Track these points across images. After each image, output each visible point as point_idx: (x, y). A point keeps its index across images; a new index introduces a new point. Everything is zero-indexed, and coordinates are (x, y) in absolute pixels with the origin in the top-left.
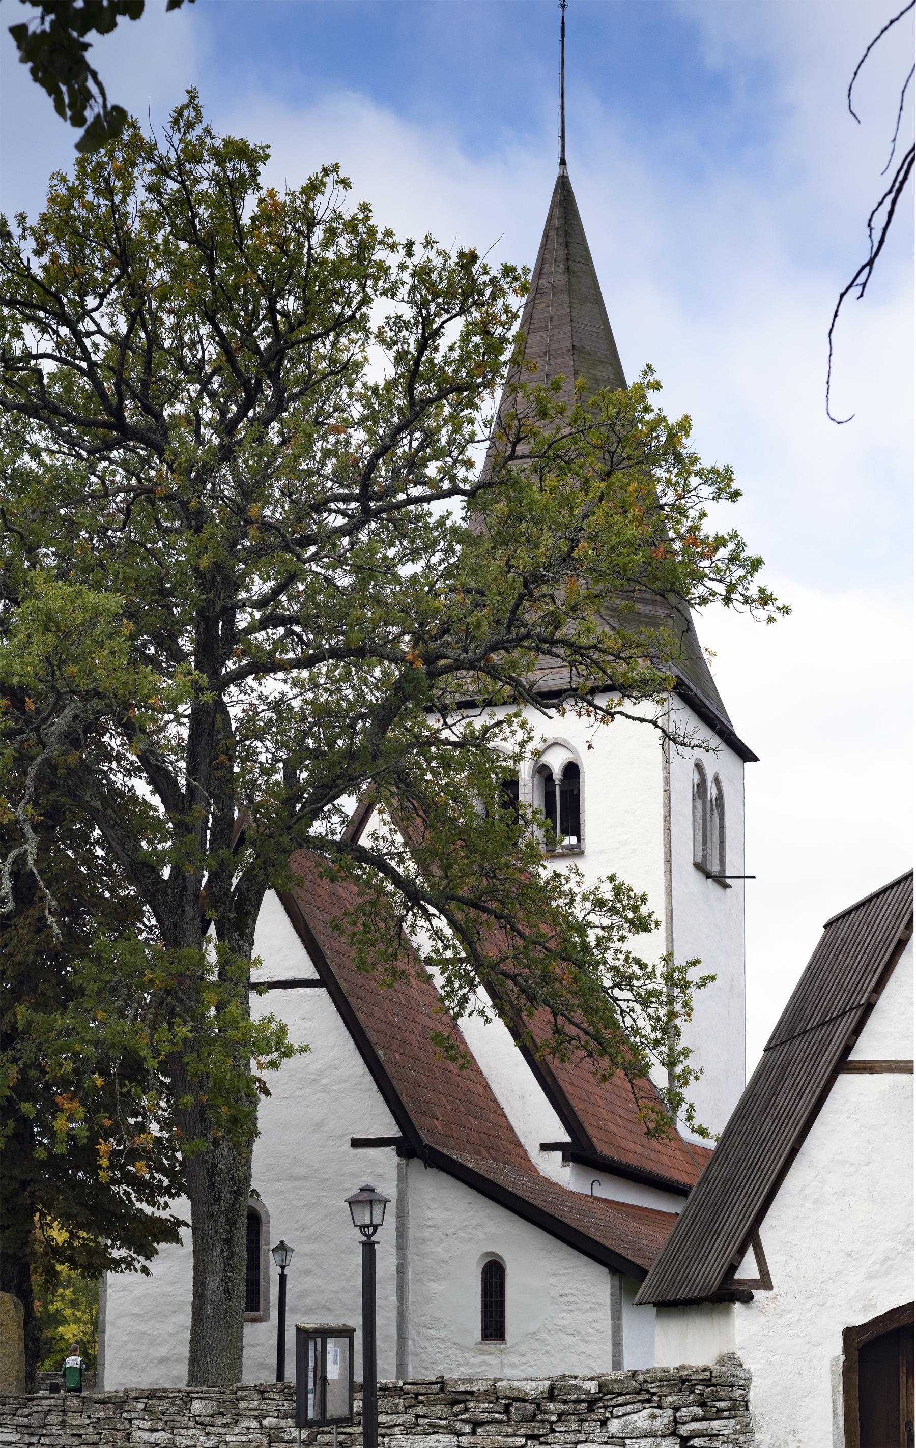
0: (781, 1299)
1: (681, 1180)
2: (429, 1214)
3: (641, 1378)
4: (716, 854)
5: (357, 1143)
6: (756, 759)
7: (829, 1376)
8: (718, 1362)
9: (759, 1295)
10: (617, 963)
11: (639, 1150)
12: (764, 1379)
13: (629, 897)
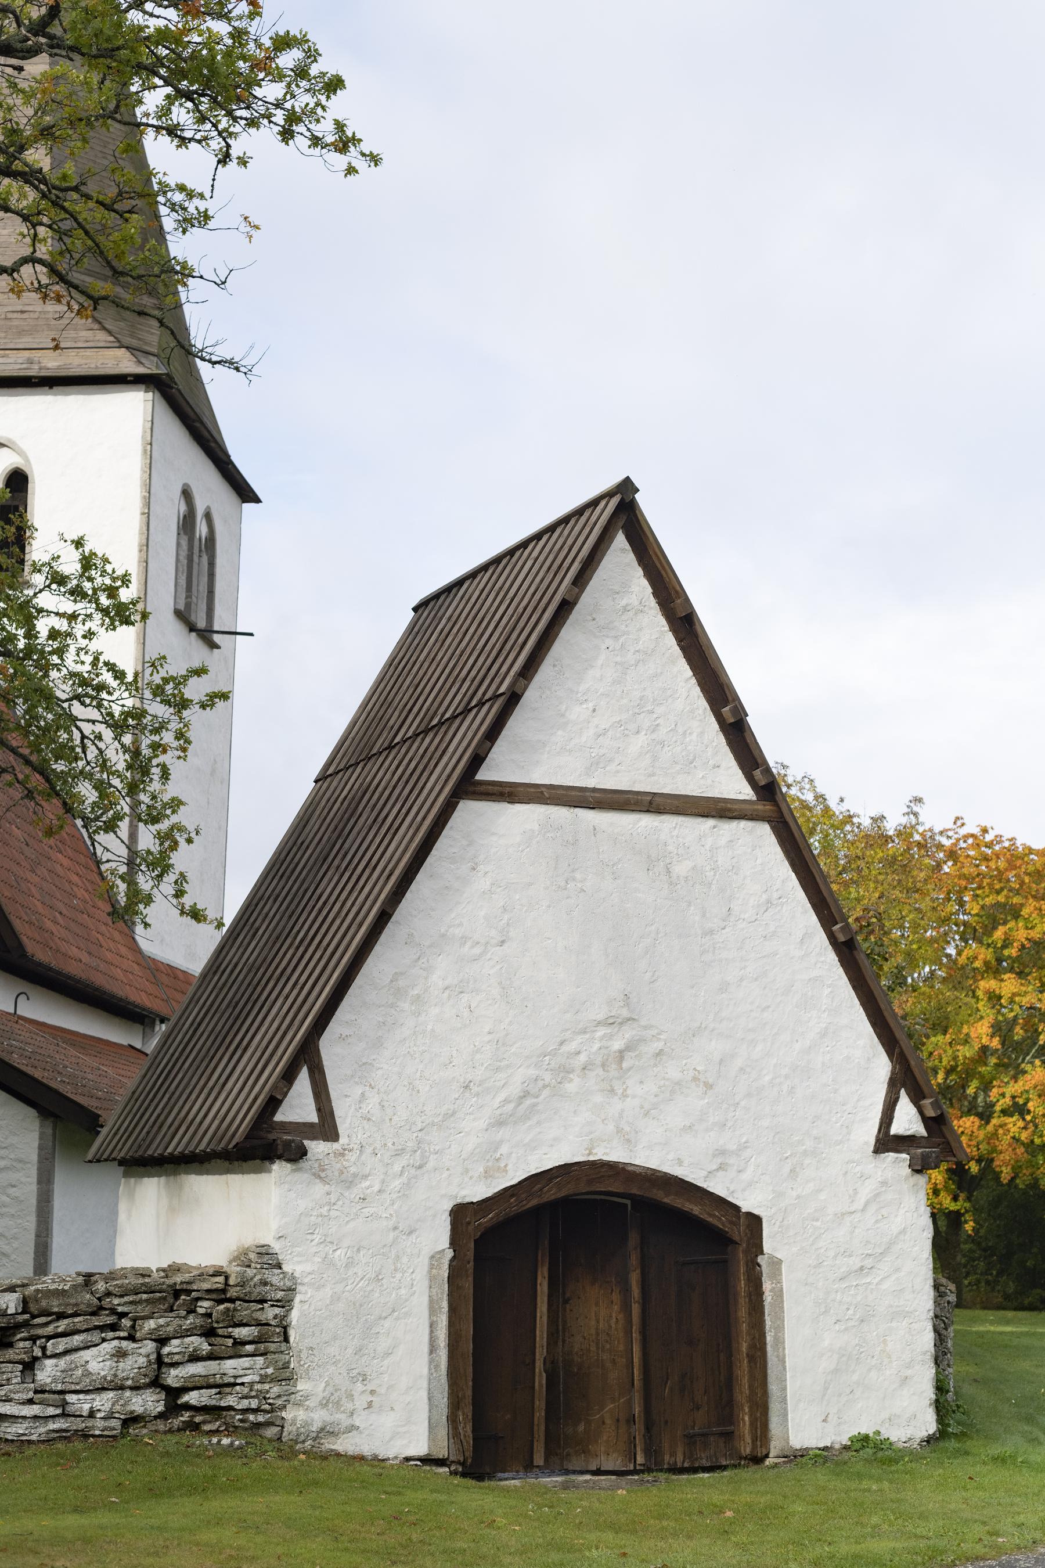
0: (352, 1157)
1: (138, 1001)
3: (101, 1287)
4: (203, 606)
6: (258, 500)
7: (426, 1283)
8: (235, 1259)
9: (317, 1148)
10: (79, 668)
11: (85, 957)
12: (318, 1289)
13: (104, 573)
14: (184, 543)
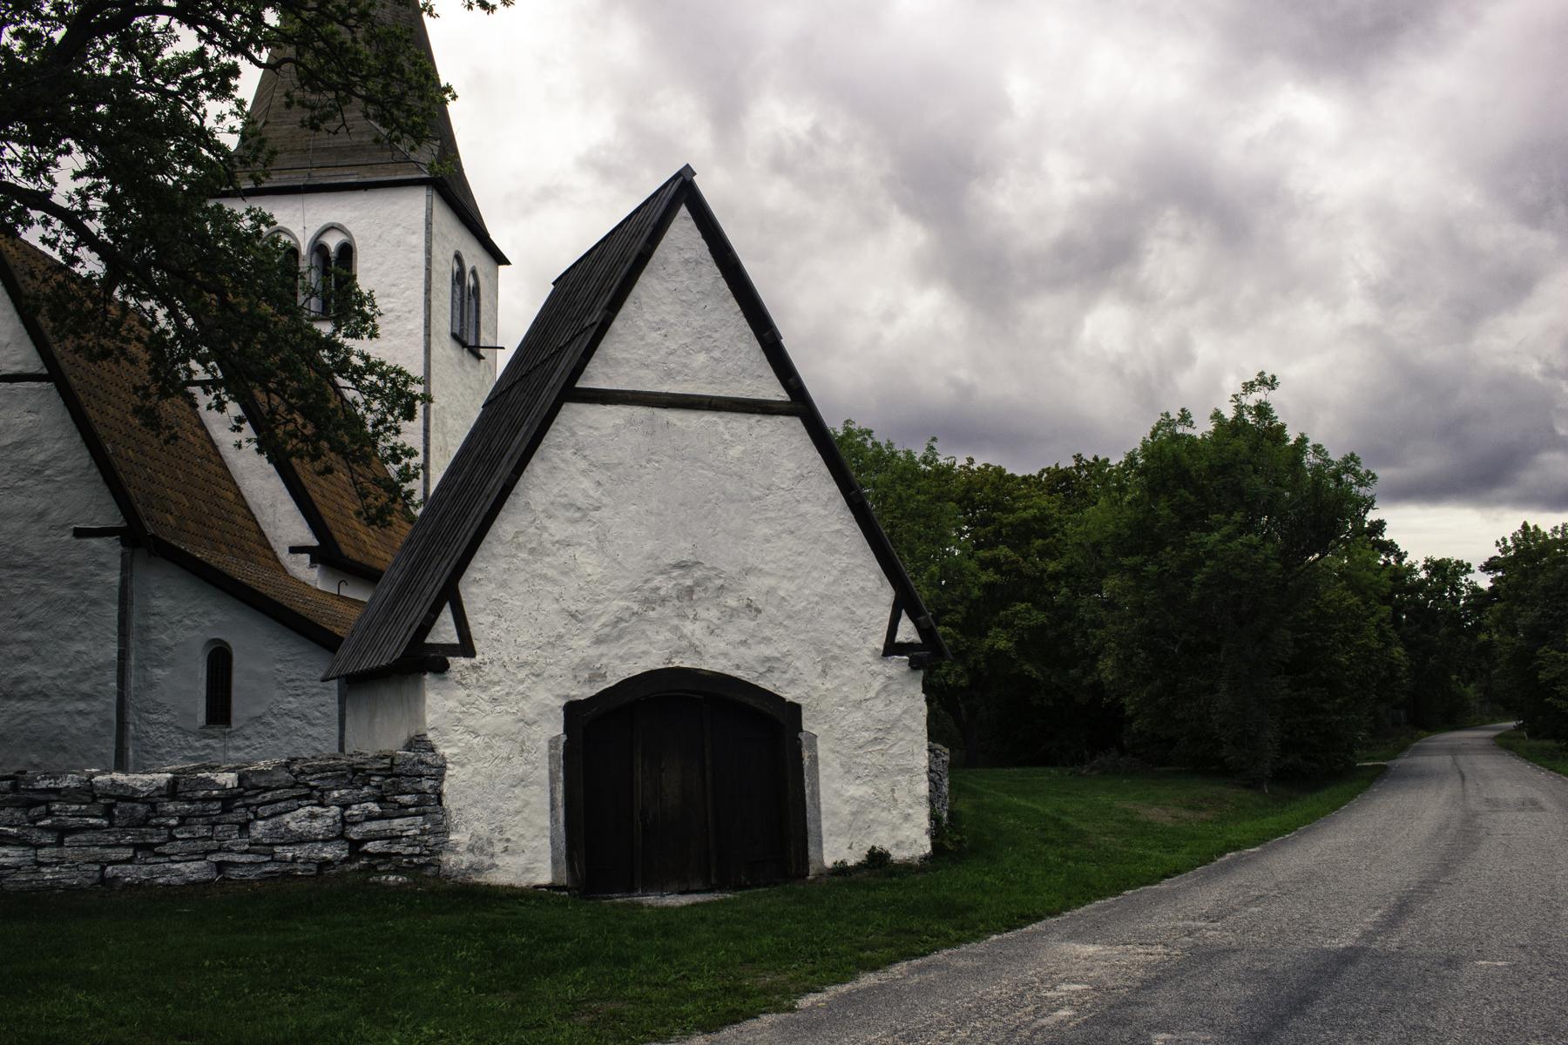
2: (155, 602)
5: (79, 533)
6: (507, 263)
9: (458, 663)
14: (458, 290)
